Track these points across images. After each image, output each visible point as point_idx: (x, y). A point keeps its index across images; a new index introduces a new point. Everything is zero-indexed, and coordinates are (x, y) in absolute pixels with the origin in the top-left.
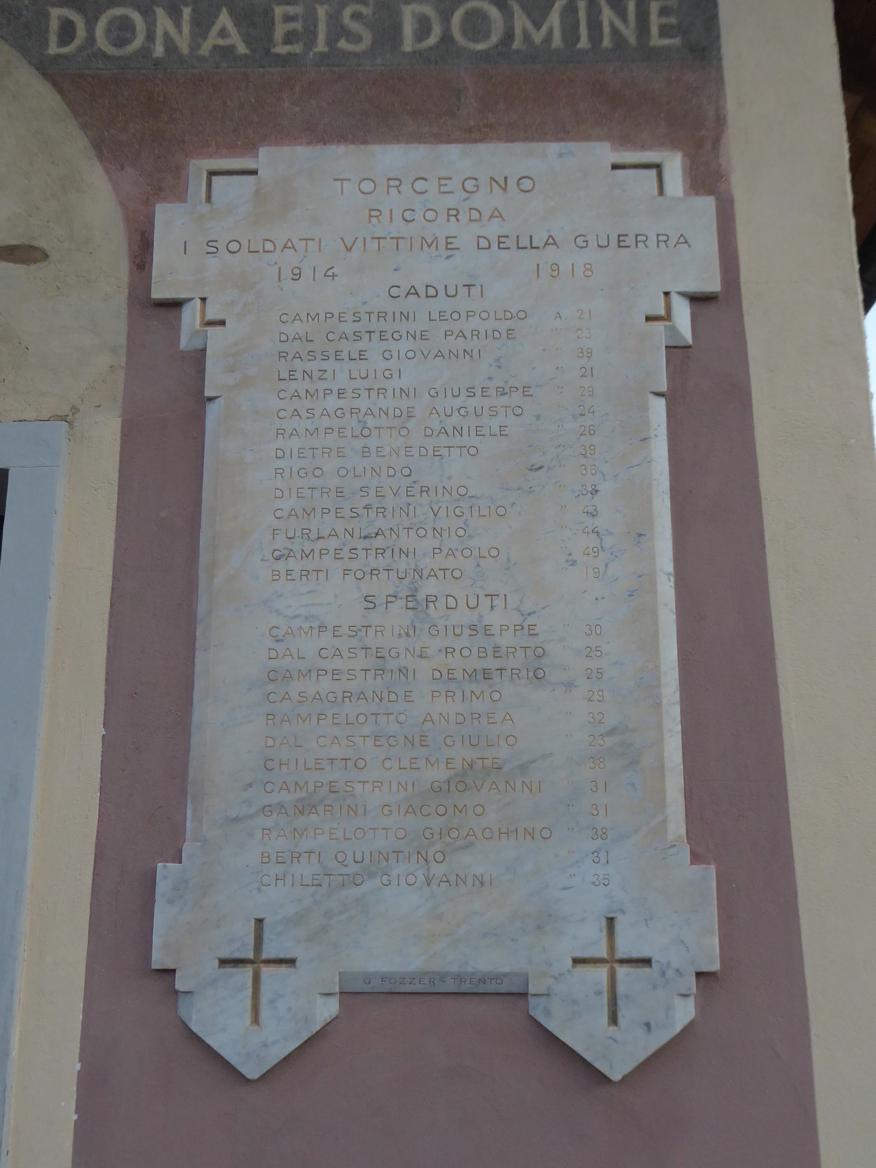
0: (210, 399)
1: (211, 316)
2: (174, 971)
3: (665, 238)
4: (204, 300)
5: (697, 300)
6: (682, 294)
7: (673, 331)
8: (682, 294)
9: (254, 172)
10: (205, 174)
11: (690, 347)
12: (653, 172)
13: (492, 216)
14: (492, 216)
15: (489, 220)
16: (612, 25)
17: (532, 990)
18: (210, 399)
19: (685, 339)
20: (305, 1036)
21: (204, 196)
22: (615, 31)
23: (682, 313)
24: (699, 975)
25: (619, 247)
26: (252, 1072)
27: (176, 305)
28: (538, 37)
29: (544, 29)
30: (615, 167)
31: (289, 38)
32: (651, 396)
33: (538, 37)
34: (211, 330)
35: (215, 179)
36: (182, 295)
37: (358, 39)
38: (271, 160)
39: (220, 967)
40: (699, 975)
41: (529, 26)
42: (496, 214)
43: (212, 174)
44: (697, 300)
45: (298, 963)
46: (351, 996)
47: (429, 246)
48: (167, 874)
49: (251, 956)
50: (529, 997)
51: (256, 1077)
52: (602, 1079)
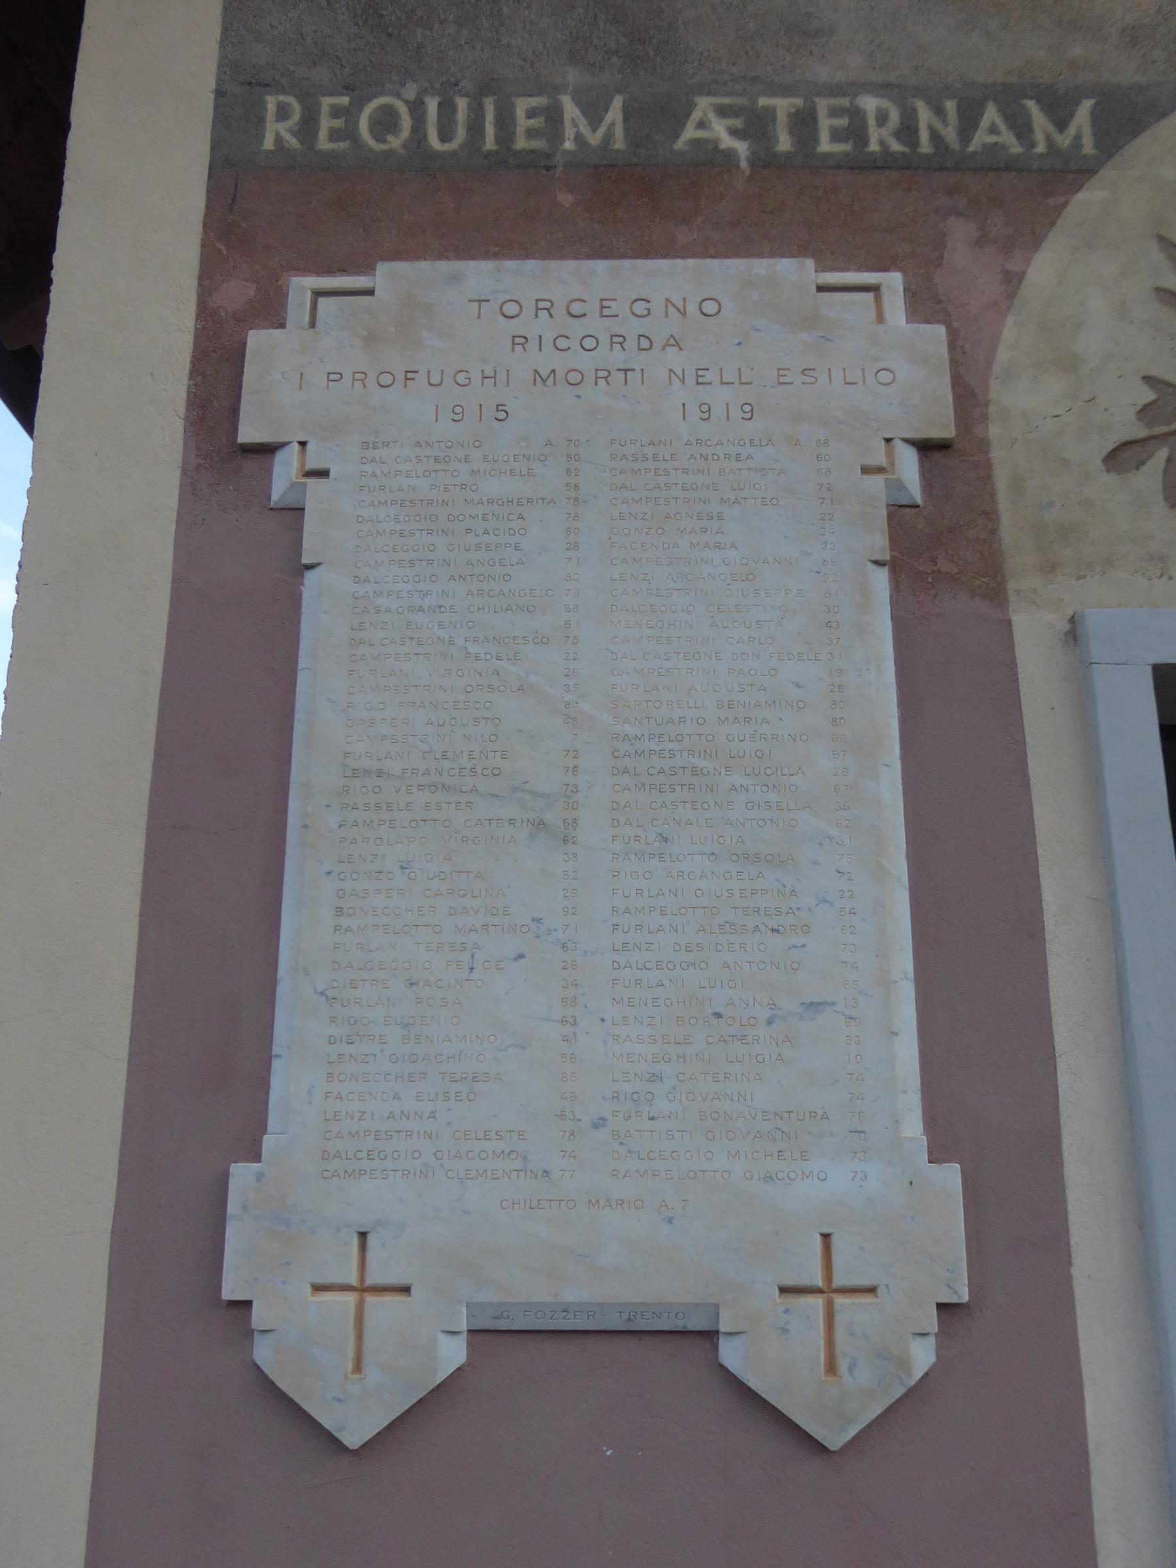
0: (309, 567)
1: (311, 465)
2: (248, 1304)
3: (606, 374)
4: (303, 444)
5: (926, 448)
6: (907, 441)
7: (899, 485)
8: (907, 441)
9: (370, 292)
10: (309, 294)
11: (918, 507)
12: (870, 296)
13: (667, 345)
14: (667, 345)
15: (663, 349)
16: (1079, 128)
17: (723, 1328)
18: (309, 567)
19: (912, 498)
20: (898, 1392)
21: (307, 319)
22: (935, 136)
23: (909, 464)
24: (940, 1306)
25: (698, 383)
26: (835, 1440)
27: (267, 450)
28: (594, 139)
29: (1072, 130)
30: (821, 289)
31: (334, 135)
32: (871, 566)
33: (594, 139)
34: (311, 481)
35: (322, 301)
36: (35, 433)
37: (444, 137)
38: (388, 277)
39: (313, 1294)
40: (940, 1306)
41: (1051, 128)
42: (672, 341)
43: (318, 293)
44: (926, 448)
45: (879, 1291)
46: (481, 1337)
47: (544, 381)
48: (241, 1174)
49: (820, 1283)
50: (256, 1334)
51: (836, 1449)
52: (823, 1449)
